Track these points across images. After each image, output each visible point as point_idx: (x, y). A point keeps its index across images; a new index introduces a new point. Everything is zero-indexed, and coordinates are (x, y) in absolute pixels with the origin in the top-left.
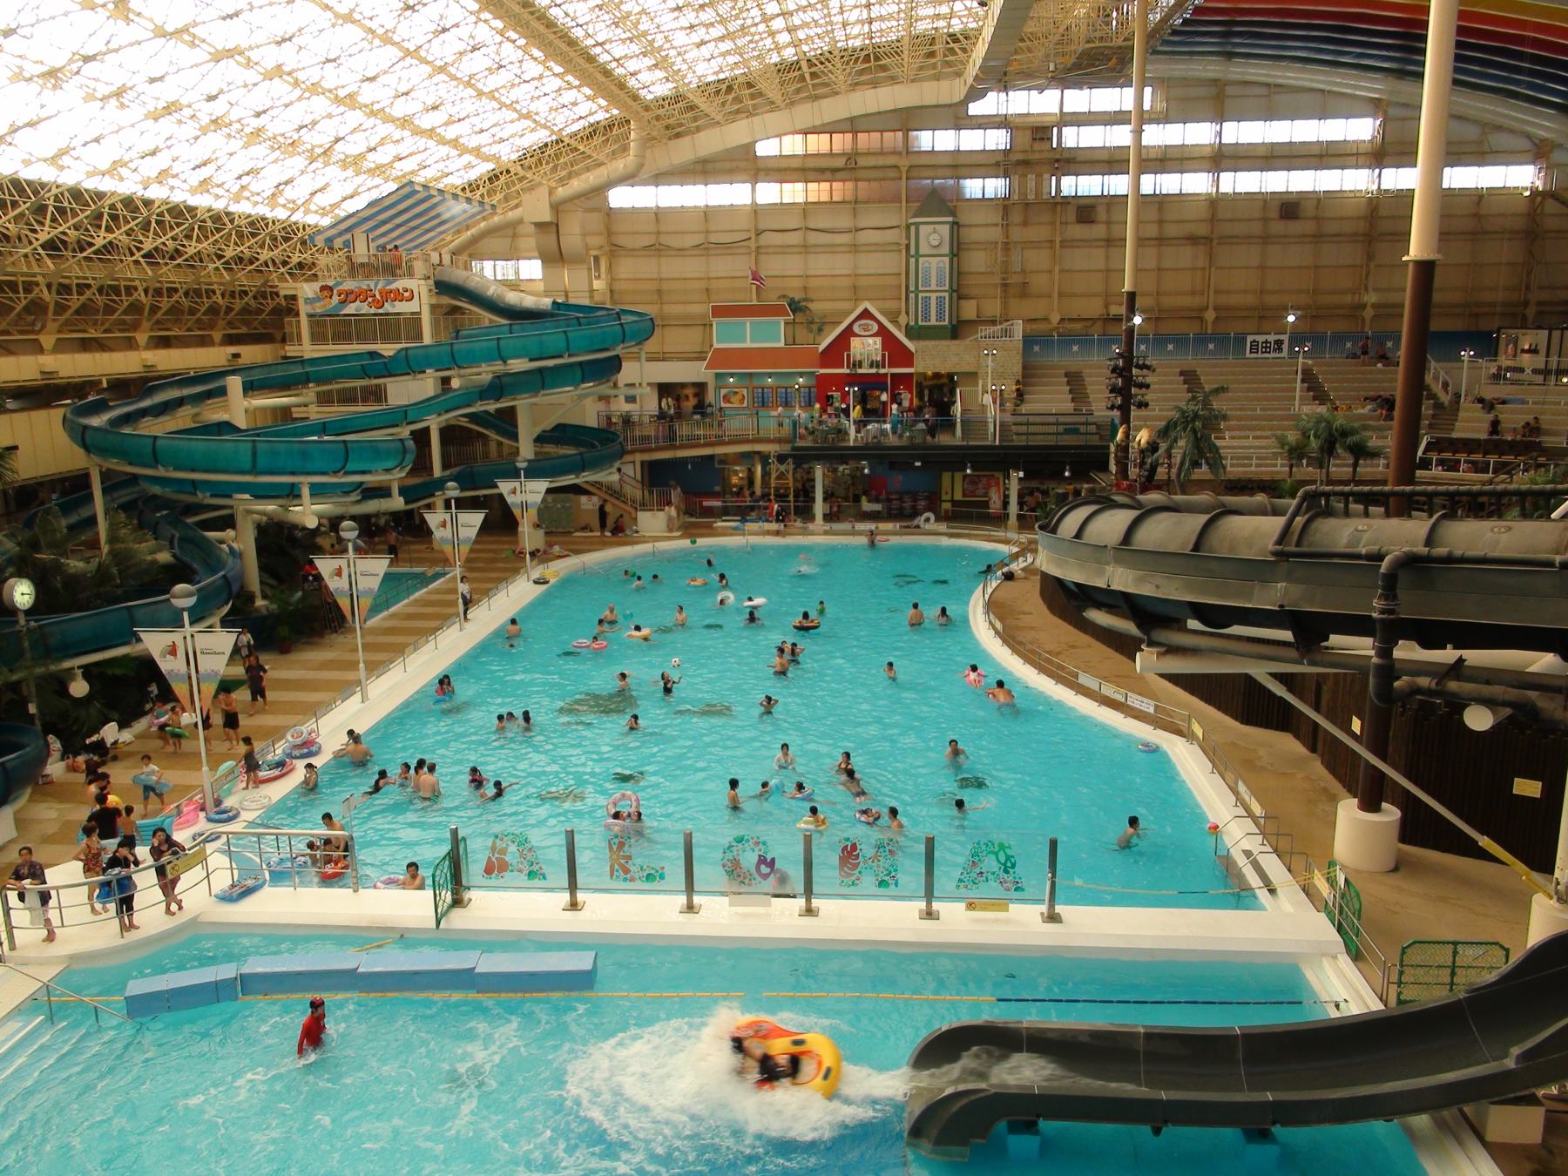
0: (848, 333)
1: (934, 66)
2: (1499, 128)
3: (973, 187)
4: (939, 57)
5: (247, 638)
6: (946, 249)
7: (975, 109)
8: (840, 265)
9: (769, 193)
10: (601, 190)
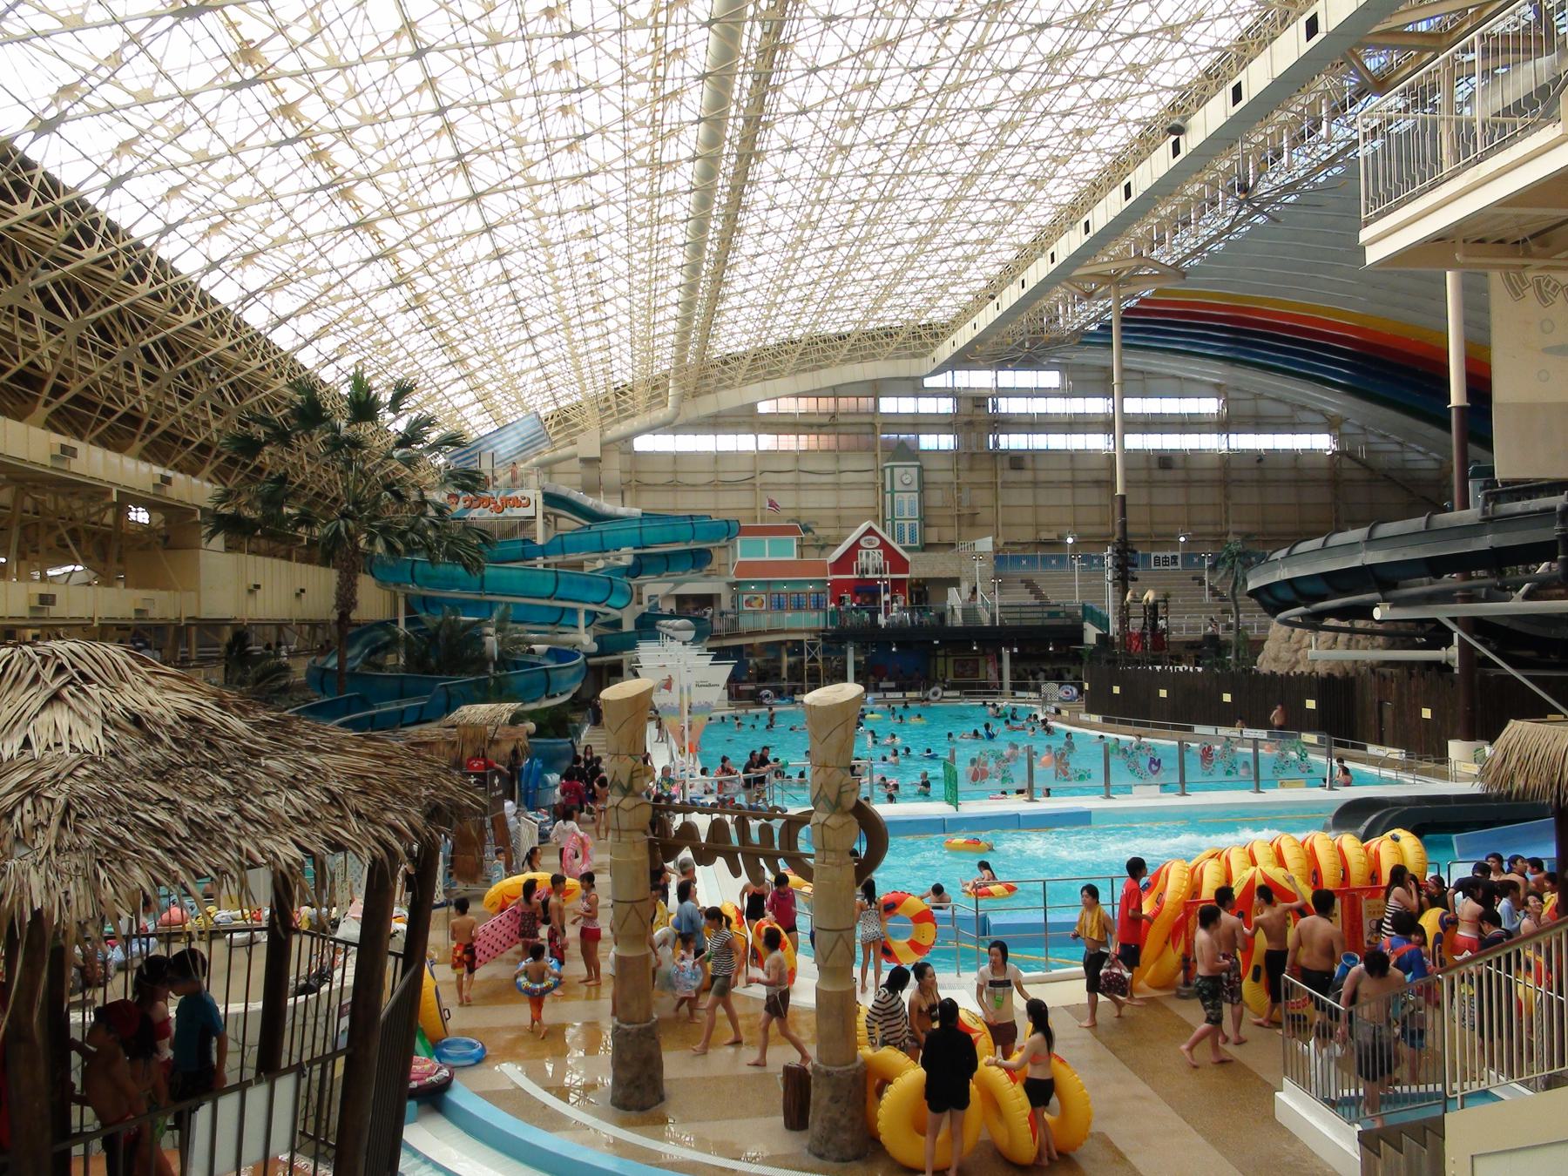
0: (856, 546)
1: (612, 415)
2: (1303, 408)
3: (928, 442)
4: (614, 408)
5: (651, 731)
6: (915, 487)
7: (929, 382)
8: (827, 499)
9: (767, 442)
10: (628, 439)
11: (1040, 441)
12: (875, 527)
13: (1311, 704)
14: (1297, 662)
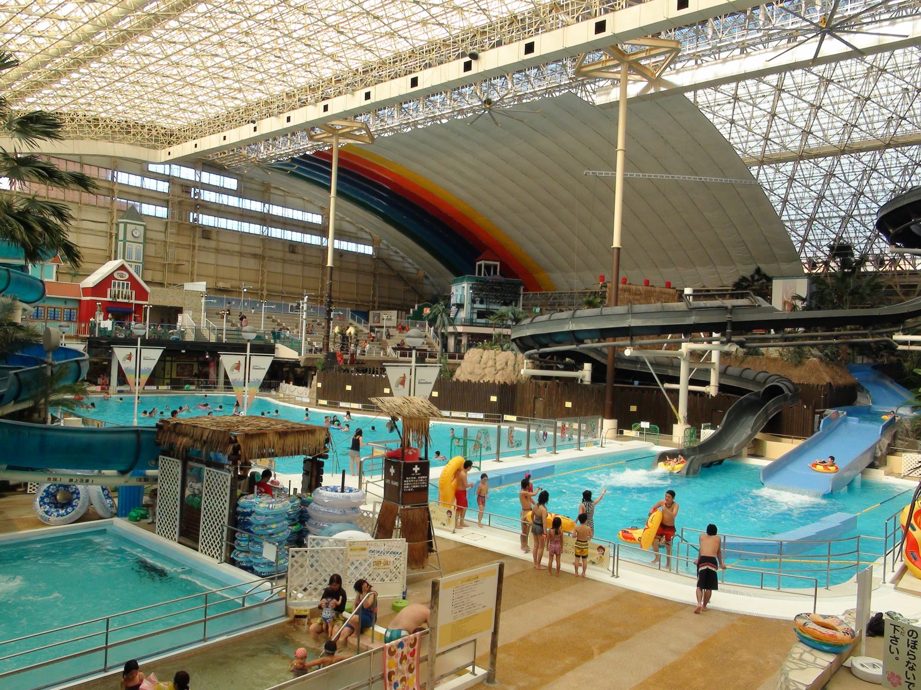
3: (148, 209)
7: (152, 168)
11: (223, 223)
12: (126, 265)
13: (494, 399)
14: (485, 375)
